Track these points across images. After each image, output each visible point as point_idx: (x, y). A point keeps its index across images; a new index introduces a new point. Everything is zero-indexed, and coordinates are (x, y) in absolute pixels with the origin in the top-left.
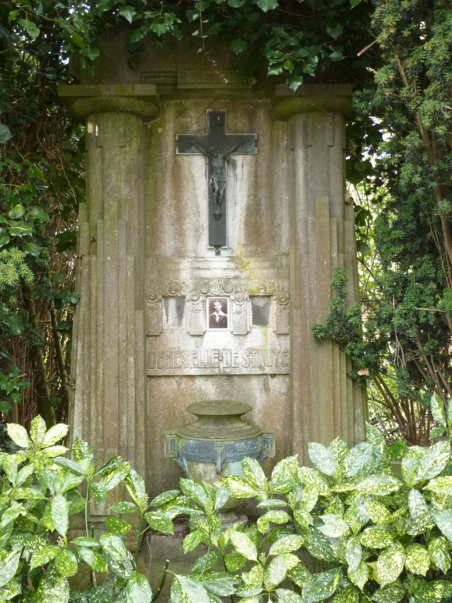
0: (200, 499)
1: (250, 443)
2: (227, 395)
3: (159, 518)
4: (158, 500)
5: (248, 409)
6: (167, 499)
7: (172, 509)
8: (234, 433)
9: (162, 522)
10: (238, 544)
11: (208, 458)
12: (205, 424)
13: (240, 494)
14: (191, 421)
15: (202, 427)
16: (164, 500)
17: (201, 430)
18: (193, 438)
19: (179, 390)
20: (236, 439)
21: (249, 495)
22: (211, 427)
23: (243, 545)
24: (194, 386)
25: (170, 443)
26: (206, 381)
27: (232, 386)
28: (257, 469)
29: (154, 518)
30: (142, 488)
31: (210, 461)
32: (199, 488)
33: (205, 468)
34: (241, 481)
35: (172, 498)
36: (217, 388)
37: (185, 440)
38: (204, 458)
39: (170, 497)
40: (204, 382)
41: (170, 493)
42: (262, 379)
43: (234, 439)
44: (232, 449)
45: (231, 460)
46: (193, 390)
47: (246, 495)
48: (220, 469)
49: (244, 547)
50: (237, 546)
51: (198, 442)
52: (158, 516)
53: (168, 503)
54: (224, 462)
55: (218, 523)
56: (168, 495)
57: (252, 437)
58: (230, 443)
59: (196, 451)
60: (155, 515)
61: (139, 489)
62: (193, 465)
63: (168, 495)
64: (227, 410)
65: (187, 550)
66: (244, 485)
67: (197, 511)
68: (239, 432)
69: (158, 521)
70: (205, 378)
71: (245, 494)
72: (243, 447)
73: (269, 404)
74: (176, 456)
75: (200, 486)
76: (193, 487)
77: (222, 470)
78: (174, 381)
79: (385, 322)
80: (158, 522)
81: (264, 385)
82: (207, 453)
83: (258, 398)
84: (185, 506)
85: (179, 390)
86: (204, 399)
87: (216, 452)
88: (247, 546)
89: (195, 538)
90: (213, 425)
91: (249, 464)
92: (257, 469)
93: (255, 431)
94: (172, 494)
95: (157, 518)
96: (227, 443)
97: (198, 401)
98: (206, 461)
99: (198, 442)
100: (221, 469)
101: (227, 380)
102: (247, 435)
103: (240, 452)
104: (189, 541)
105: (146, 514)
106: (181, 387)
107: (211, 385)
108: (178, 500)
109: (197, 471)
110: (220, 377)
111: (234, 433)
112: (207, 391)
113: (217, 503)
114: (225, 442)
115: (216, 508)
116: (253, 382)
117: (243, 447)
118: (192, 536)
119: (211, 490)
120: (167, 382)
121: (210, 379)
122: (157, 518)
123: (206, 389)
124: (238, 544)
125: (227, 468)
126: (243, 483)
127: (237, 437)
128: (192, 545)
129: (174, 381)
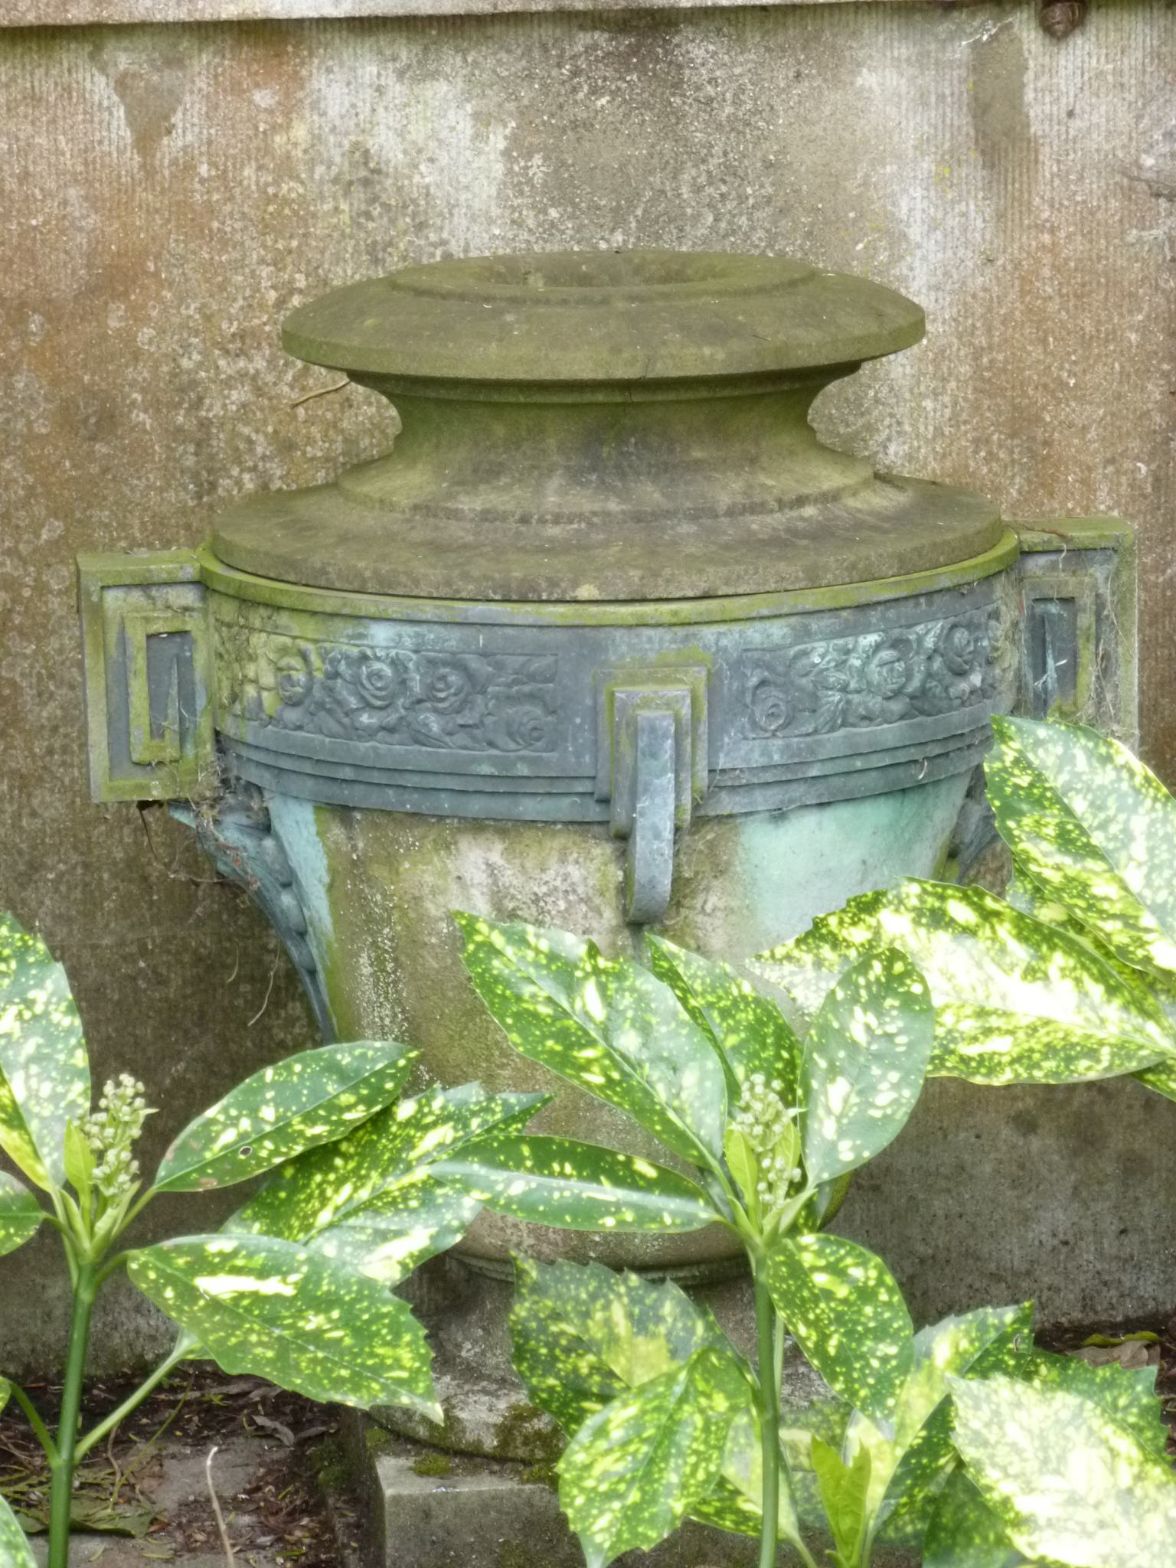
0: (661, 1094)
1: (930, 634)
2: (619, 218)
3: (271, 1286)
4: (229, 1136)
5: (903, 321)
6: (310, 1118)
7: (367, 1207)
8: (782, 543)
9: (314, 1322)
10: (1029, 1489)
11: (555, 784)
12: (487, 474)
13: (1001, 1046)
14: (276, 469)
15: (470, 503)
16: (282, 1133)
17: (458, 532)
18: (394, 607)
19: (149, 171)
20: (810, 600)
21: (1092, 1054)
22: (552, 500)
23: (1073, 1500)
24: (300, 132)
25: (140, 662)
26: (418, 74)
27: (671, 120)
28: (1139, 823)
29: (219, 1286)
30: (51, 1038)
31: (564, 807)
32: (642, 999)
33: (509, 876)
34: (1005, 930)
35: (358, 1114)
36: (517, 149)
37: (309, 628)
38: (510, 786)
39: (333, 1107)
40: (397, 90)
41: (333, 1068)
42: (961, 49)
43: (788, 603)
44: (774, 695)
45: (763, 800)
46: (285, 168)
47: (1069, 1052)
48: (665, 884)
49: (1088, 1516)
50: (1022, 1505)
51: (453, 639)
52: (262, 1273)
53: (318, 1157)
54: (700, 821)
55: (866, 1294)
56: (317, 1091)
57: (945, 578)
58: (755, 634)
59: (435, 725)
60: (225, 1264)
61: (30, 1047)
62: (391, 861)
63: (317, 1091)
64: (717, 333)
65: (603, 1540)
66: (1030, 972)
67: (654, 1200)
68: (821, 534)
69: (268, 1311)
70: (405, 52)
71: (1050, 1050)
72: (875, 672)
73: (1026, 285)
74: (206, 782)
75: (649, 983)
76: (590, 989)
77: (681, 887)
78: (99, 87)
79: (287, 114)
80: (271, 1321)
81: (980, 109)
82: (532, 736)
83: (915, 233)
84: (542, 1164)
85: (149, 171)
86: (394, 262)
87: (632, 723)
88: (1111, 1509)
89: (668, 1432)
90: (575, 476)
91: (1057, 781)
92: (1139, 823)
93: (955, 529)
94: (346, 1077)
95: (248, 1284)
96: (731, 637)
97: (345, 273)
98: (528, 808)
99: (453, 639)
100: (677, 880)
101: (621, 61)
102: (905, 565)
103: (844, 718)
104: (613, 1464)
105: (138, 1259)
106: (171, 146)
107: (460, 122)
108: (416, 1123)
109: (432, 909)
110: (547, 33)
111: (782, 543)
112: (427, 175)
113: (826, 1127)
114: (709, 633)
115: (818, 1172)
116: (867, 79)
117: (875, 672)
118: (637, 1425)
119: (747, 1016)
120: (34, 99)
121: (451, 60)
122: (248, 1284)
123: (416, 154)
124: (1029, 1489)
125: (721, 871)
126: (1020, 953)
127: (813, 581)
128: (649, 1499)
129: (99, 87)
